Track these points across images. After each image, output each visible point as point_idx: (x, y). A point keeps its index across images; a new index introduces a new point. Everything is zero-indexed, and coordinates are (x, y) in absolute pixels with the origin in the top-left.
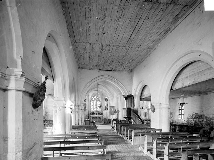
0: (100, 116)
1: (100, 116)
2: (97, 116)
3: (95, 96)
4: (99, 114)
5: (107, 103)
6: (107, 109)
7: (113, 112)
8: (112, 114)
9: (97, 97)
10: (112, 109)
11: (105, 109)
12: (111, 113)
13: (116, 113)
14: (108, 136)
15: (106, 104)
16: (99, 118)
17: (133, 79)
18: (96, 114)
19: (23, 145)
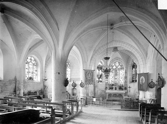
0: (121, 92)
1: (121, 92)
2: (118, 91)
3: (117, 63)
4: (121, 88)
5: (136, 71)
6: (136, 81)
7: (145, 86)
8: (143, 90)
9: (119, 63)
10: (142, 80)
11: (133, 81)
12: (141, 88)
13: (152, 88)
14: (53, 30)
15: (134, 73)
16: (120, 95)
17: (97, 17)
18: (116, 89)
19: (21, 55)
